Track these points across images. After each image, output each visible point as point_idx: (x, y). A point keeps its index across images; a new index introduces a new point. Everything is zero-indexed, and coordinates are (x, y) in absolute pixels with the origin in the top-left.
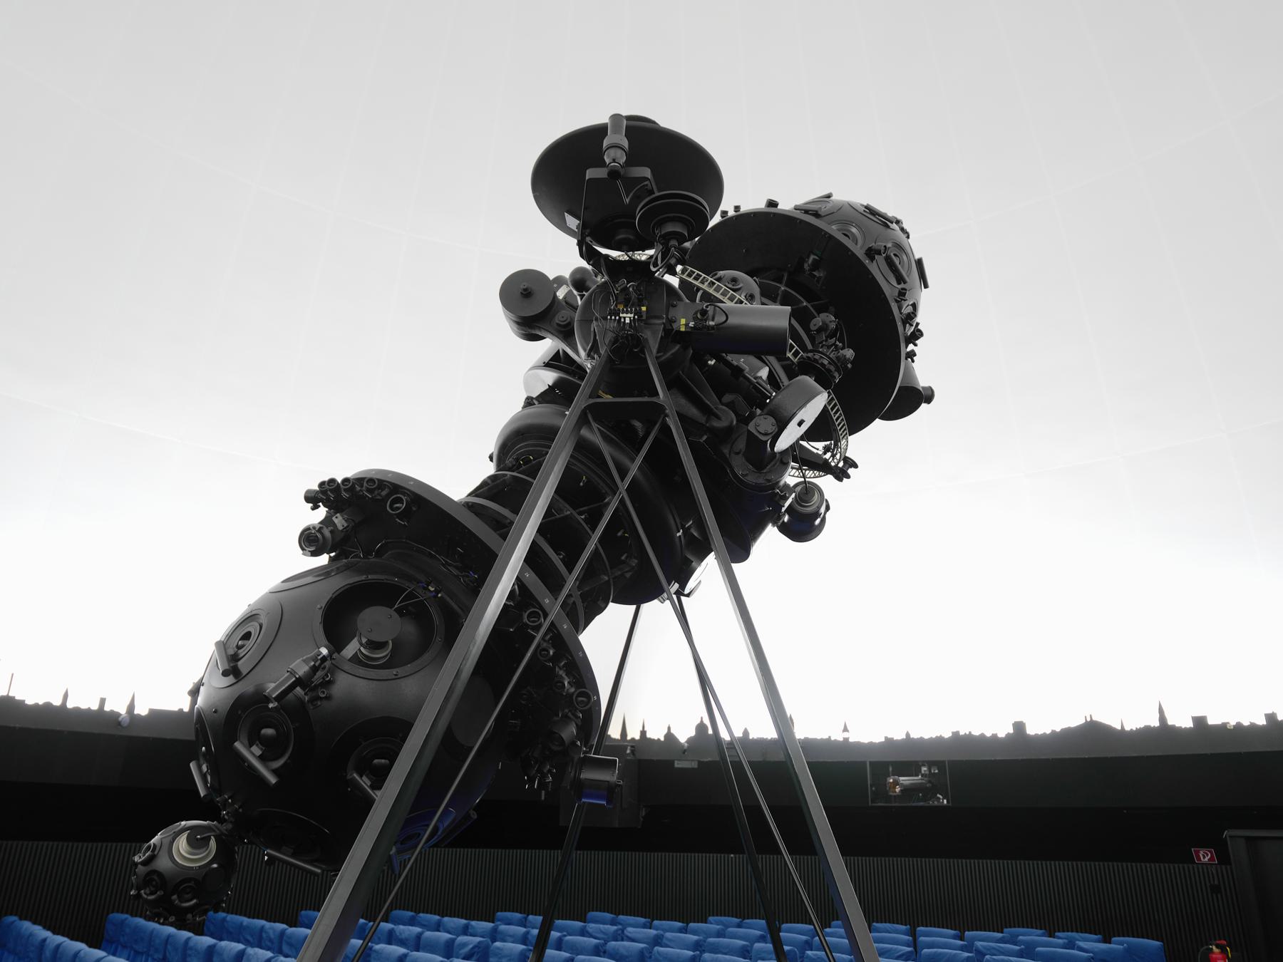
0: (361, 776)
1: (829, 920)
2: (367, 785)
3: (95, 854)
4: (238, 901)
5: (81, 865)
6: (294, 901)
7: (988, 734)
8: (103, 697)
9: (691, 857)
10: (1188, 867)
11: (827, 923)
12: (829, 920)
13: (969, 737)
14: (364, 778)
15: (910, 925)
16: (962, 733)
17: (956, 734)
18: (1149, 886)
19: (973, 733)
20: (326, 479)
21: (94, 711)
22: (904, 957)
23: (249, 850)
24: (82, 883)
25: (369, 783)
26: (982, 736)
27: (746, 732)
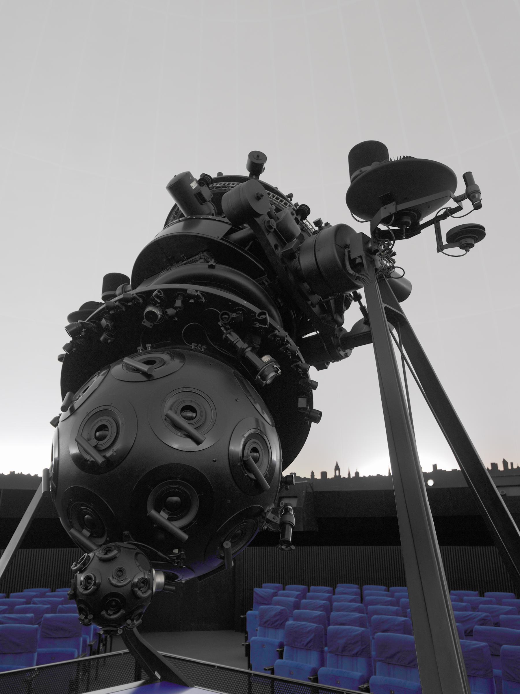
0: (159, 512)
1: (22, 588)
2: (164, 518)
3: (41, 554)
4: (476, 558)
5: (24, 560)
6: (396, 562)
7: (32, 474)
8: (434, 464)
9: (343, 549)
10: (468, 548)
11: (54, 589)
12: (22, 588)
13: (21, 475)
14: (162, 513)
15: (6, 593)
16: (16, 473)
17: (12, 473)
18: (494, 559)
19: (23, 473)
20: (486, 232)
21: (432, 472)
22: (327, 592)
23: (30, 552)
24: (302, 557)
25: (166, 516)
26: (29, 475)
27: (357, 473)
